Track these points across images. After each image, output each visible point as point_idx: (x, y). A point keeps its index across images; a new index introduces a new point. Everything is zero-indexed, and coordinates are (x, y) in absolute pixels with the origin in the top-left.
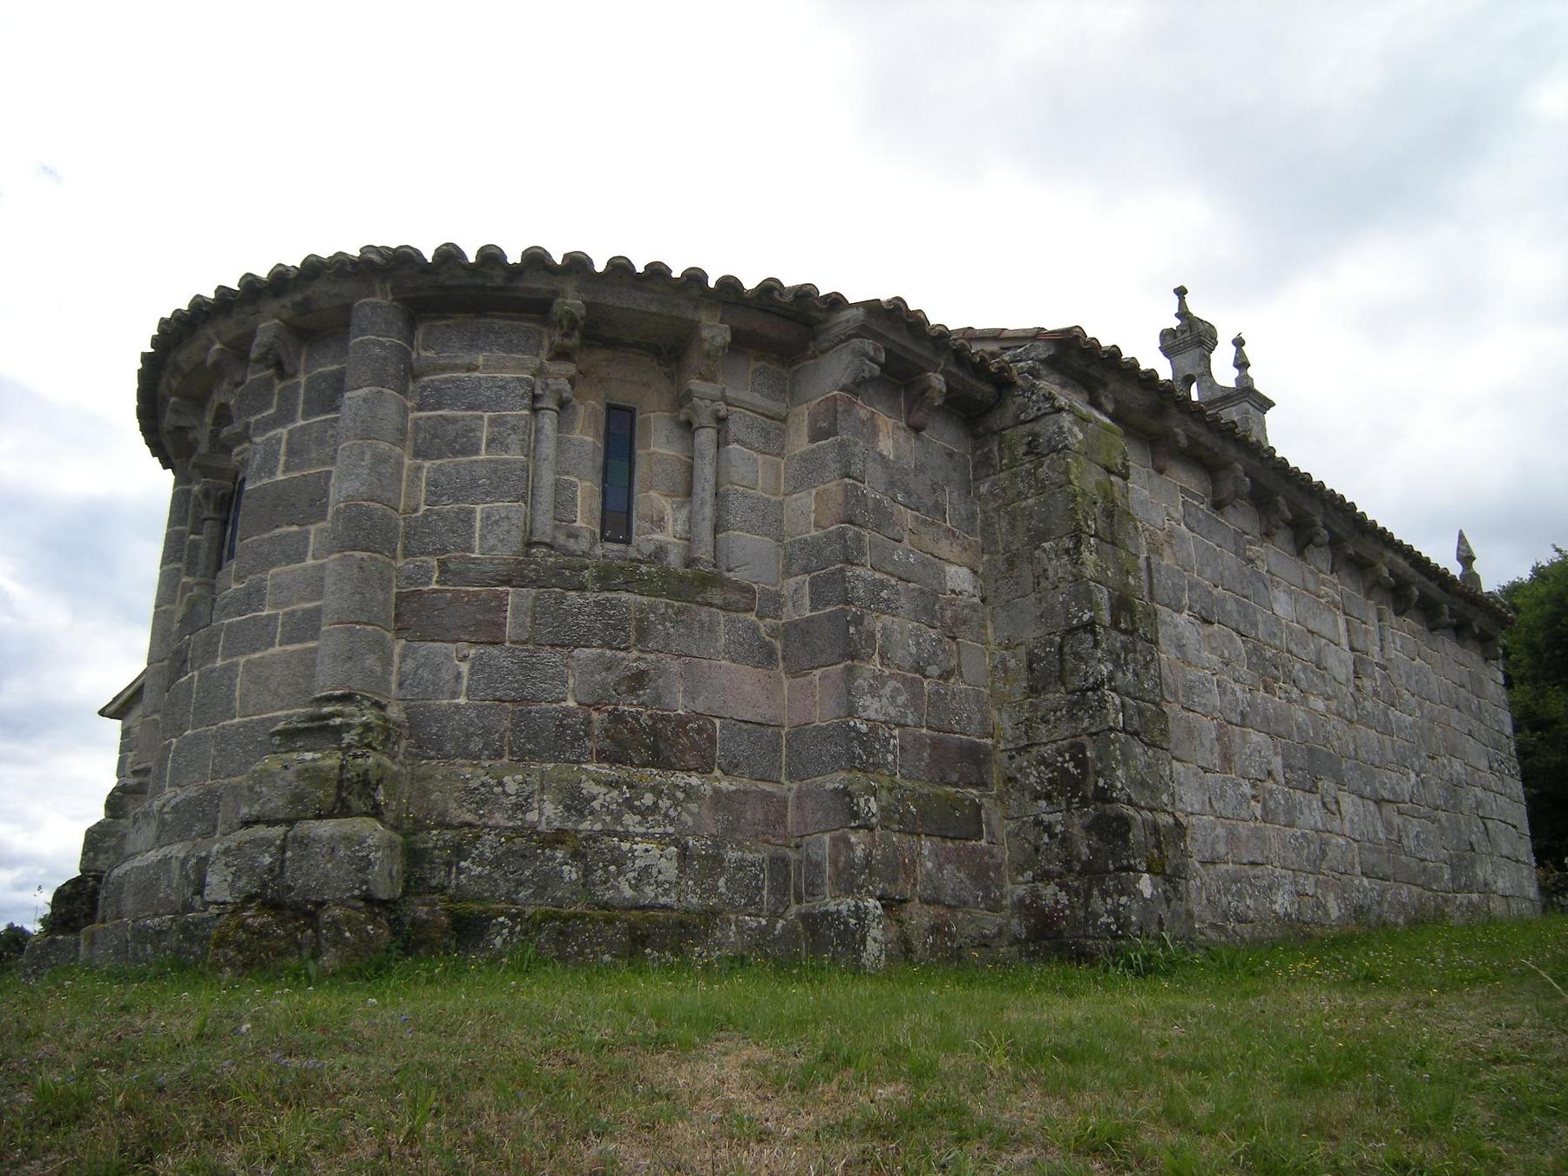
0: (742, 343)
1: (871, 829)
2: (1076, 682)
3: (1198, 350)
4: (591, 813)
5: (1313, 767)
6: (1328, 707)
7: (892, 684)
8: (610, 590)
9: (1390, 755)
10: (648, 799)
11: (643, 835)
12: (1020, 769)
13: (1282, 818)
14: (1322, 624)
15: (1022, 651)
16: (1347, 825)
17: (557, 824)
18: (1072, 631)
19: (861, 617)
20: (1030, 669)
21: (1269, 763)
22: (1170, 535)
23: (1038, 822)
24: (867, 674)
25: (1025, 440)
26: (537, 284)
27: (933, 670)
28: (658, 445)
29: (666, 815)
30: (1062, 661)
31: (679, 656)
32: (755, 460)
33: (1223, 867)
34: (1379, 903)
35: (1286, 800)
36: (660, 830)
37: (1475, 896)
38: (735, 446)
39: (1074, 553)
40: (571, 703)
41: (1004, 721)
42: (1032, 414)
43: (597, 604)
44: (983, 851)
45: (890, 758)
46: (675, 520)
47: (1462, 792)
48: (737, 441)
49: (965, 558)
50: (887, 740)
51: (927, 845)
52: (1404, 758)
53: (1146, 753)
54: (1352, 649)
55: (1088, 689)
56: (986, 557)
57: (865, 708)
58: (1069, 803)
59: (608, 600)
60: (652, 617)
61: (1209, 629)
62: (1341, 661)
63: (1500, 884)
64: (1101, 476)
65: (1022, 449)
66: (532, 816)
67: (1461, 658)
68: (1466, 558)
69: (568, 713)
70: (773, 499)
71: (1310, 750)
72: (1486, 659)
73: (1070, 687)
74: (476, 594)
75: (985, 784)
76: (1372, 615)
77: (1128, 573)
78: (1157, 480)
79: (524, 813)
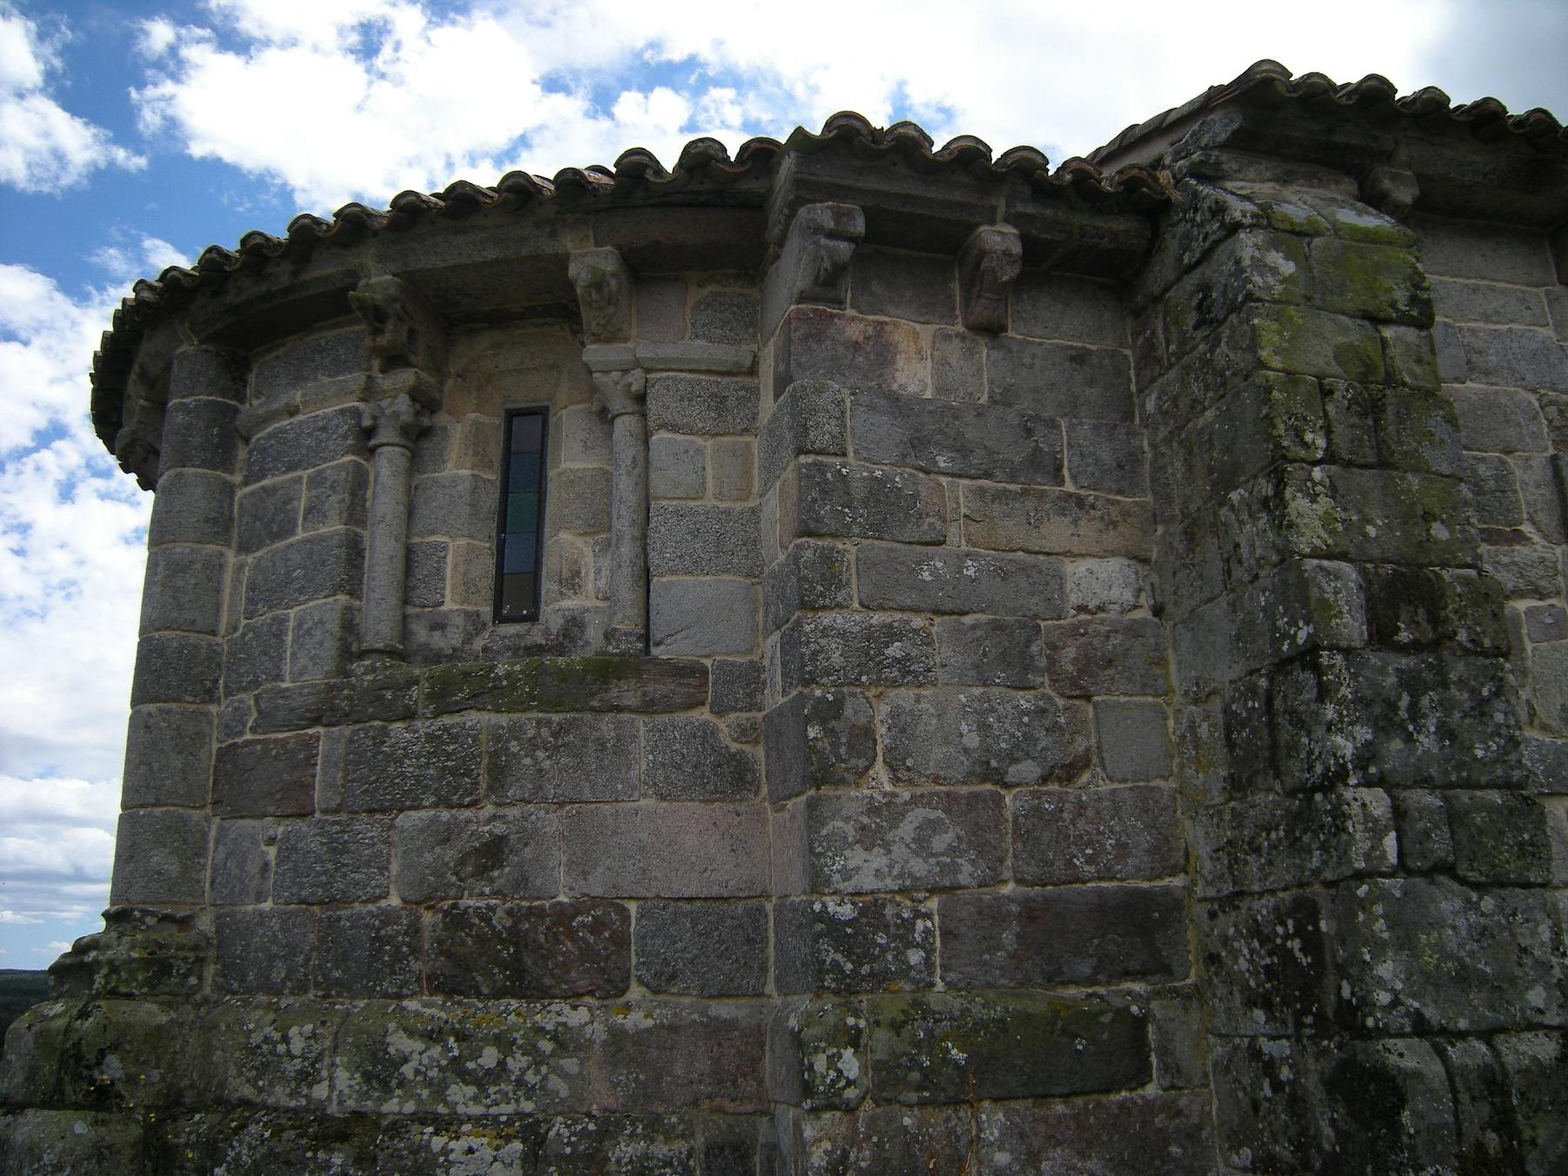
0: (647, 270)
1: (850, 1109)
2: (1295, 771)
4: (401, 1085)
7: (918, 815)
8: (451, 712)
10: (490, 1057)
11: (478, 1121)
12: (1225, 941)
15: (1216, 705)
17: (351, 1103)
18: (1283, 666)
19: (838, 705)
20: (1230, 744)
23: (1255, 1053)
24: (851, 808)
25: (1194, 302)
26: (325, 269)
27: (1027, 770)
28: (572, 457)
29: (520, 1083)
30: (1272, 727)
31: (561, 805)
32: (699, 451)
36: (509, 1109)
38: (664, 434)
39: (1274, 506)
40: (394, 901)
41: (1198, 838)
42: (1198, 247)
43: (431, 737)
44: (1149, 1107)
45: (915, 957)
46: (598, 571)
48: (663, 426)
49: (1112, 539)
50: (909, 925)
51: (993, 1120)
53: (1470, 906)
55: (1316, 788)
56: (1160, 530)
57: (847, 874)
58: (1299, 1025)
59: (446, 729)
60: (514, 746)
64: (1354, 334)
65: (1191, 319)
66: (320, 1091)
69: (388, 917)
70: (739, 506)
73: (1288, 781)
74: (285, 741)
75: (1167, 970)
77: (1428, 517)
79: (310, 1086)
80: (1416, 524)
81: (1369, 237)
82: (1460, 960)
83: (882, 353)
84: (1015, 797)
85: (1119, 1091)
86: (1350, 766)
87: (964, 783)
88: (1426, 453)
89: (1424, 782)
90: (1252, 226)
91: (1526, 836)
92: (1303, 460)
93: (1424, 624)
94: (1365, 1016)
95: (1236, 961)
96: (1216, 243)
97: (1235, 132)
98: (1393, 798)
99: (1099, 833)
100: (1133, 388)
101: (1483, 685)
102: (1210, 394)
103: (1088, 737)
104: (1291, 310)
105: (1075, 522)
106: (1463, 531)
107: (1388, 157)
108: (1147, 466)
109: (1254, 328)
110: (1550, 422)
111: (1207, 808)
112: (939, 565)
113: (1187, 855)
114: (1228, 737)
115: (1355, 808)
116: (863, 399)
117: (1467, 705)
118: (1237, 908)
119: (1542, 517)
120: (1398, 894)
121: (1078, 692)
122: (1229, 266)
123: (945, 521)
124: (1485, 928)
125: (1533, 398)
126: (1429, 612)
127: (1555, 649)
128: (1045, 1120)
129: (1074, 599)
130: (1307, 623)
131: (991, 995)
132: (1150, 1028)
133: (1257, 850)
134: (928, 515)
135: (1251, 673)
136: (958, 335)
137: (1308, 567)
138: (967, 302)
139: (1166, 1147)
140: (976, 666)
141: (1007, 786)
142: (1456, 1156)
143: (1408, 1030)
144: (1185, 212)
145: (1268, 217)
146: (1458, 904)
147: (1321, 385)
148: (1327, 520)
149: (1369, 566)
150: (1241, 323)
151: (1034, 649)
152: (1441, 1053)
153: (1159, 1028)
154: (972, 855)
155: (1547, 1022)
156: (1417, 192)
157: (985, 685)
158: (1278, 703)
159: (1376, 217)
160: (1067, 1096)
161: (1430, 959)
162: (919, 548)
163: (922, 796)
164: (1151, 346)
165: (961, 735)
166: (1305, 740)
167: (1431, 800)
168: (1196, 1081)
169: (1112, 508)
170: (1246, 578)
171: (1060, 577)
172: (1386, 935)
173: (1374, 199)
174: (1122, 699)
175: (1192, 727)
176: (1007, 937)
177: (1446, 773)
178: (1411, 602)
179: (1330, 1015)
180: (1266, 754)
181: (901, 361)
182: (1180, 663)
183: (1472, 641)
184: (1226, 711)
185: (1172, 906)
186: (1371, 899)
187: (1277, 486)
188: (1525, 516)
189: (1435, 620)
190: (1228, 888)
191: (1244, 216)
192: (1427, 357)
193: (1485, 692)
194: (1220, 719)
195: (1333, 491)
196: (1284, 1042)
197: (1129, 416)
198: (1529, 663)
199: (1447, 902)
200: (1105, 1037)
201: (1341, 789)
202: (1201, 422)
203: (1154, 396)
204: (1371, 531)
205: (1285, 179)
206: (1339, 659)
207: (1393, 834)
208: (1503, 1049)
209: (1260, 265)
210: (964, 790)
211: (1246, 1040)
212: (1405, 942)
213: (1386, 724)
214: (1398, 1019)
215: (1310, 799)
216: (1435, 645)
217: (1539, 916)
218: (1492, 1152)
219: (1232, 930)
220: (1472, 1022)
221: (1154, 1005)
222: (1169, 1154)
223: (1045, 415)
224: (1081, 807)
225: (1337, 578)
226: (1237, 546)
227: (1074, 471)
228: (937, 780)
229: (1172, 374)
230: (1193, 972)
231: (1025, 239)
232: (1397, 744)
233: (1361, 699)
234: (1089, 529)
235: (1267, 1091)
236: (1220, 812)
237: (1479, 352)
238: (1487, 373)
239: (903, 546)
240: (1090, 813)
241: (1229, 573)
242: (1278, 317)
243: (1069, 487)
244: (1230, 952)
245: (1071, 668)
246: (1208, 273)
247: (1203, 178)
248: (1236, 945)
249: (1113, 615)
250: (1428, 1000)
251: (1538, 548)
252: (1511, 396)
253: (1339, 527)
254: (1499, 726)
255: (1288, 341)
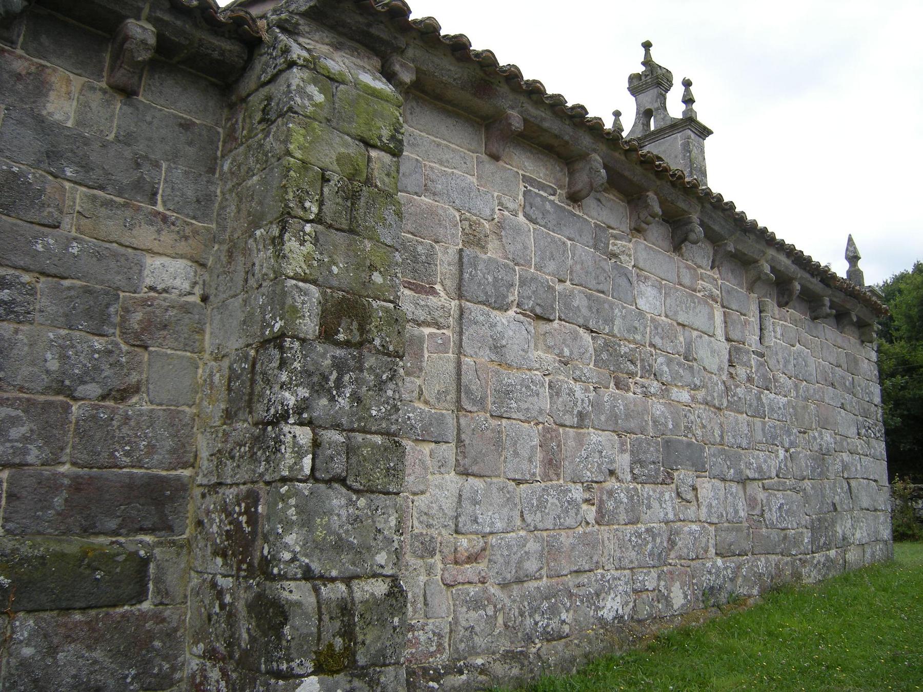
2: (260, 412)
3: (656, 90)
5: (668, 458)
6: (693, 398)
9: (759, 436)
12: (208, 512)
13: (623, 517)
14: (699, 319)
15: (226, 363)
16: (704, 510)
20: (229, 389)
21: (612, 462)
22: (501, 226)
23: (214, 585)
27: (92, 390)
30: (253, 382)
33: (532, 585)
34: (732, 580)
35: (631, 498)
37: (832, 553)
39: (277, 242)
42: (271, 71)
44: (143, 616)
47: (829, 460)
52: (774, 437)
53: (351, 503)
54: (728, 340)
55: (270, 423)
61: (544, 327)
62: (713, 351)
63: (858, 535)
64: (353, 149)
65: (258, 116)
67: (839, 341)
68: (853, 258)
71: (667, 443)
72: (863, 342)
75: (170, 529)
76: (754, 308)
77: (372, 268)
78: (490, 166)
80: (364, 271)
81: (375, 94)
82: (339, 535)
83: (40, 87)
84: (79, 407)
85: (123, 605)
86: (291, 412)
87: (42, 394)
88: (380, 230)
89: (337, 426)
90: (302, 66)
91: (392, 465)
92: (301, 218)
93: (355, 331)
94: (273, 567)
95: (211, 527)
96: (281, 72)
97: (311, 7)
98: (315, 434)
99: (136, 436)
100: (219, 154)
101: (384, 372)
102: (258, 166)
103: (141, 373)
104: (316, 124)
105: (159, 232)
106: (391, 280)
107: (402, 52)
108: (217, 205)
109: (289, 129)
110: (464, 230)
111: (211, 427)
112: (51, 241)
113: (196, 456)
114: (229, 385)
115: (289, 437)
116: (14, 114)
117: (372, 384)
118: (217, 493)
119: (448, 283)
120: (306, 493)
121: (138, 343)
122: (284, 88)
123: (61, 212)
124: (358, 516)
125: (457, 214)
126: (359, 324)
127: (440, 358)
128: (65, 625)
129: (148, 281)
130: (281, 319)
131: (39, 539)
132: (152, 565)
133: (233, 458)
134: (49, 206)
135: (248, 346)
136: (101, 89)
137: (289, 285)
138: (112, 69)
139: (151, 642)
140: (66, 315)
141: (75, 399)
142: (315, 653)
143: (299, 576)
144: (269, 48)
145: (315, 64)
146: (343, 501)
147: (323, 175)
148: (308, 258)
149: (329, 291)
150: (283, 125)
151: (112, 310)
152: (316, 590)
153: (158, 566)
154: (40, 443)
155: (385, 573)
156: (414, 78)
157: (70, 329)
158: (258, 366)
159: (384, 83)
160: (84, 609)
161: (320, 534)
162: (37, 227)
163: (8, 399)
164: (233, 129)
165: (46, 361)
166: (268, 392)
167: (337, 437)
168: (178, 600)
169: (186, 228)
170: (255, 286)
171: (141, 266)
172: (294, 518)
173: (389, 75)
174: (169, 352)
175: (211, 375)
176: (58, 501)
177: (352, 422)
178: (350, 317)
179: (256, 565)
180: (247, 398)
181: (52, 95)
182: (211, 333)
183: (383, 346)
184: (230, 368)
185: (180, 488)
186: (288, 495)
187: (281, 231)
188: (439, 280)
189: (362, 329)
190: (214, 480)
191: (299, 59)
192: (394, 174)
193: (384, 377)
194: (226, 372)
195: (316, 241)
196: (230, 579)
197: (212, 171)
198: (424, 364)
199: (337, 499)
200: (118, 570)
201: (282, 424)
202: (250, 183)
203: (229, 161)
204: (335, 269)
205: (337, 47)
206: (297, 344)
207: (310, 456)
208: (355, 588)
209: (301, 91)
210: (42, 398)
211: (211, 576)
212: (307, 522)
213: (320, 387)
214: (294, 569)
215: (265, 430)
216: (360, 345)
217: (391, 511)
218: (337, 649)
219: (212, 506)
220: (340, 572)
221: (157, 551)
222: (153, 646)
223: (152, 157)
224: (127, 419)
225: (306, 294)
226: (254, 264)
227: (165, 199)
228: (21, 389)
229: (241, 149)
230: (187, 531)
231: (160, 37)
232: (324, 401)
233: (306, 371)
234: (167, 237)
235: (217, 609)
236: (217, 431)
237: (433, 181)
238: (434, 194)
239: (25, 224)
240: (132, 423)
241: (246, 281)
242: (306, 127)
243: (160, 208)
244: (209, 520)
245: (136, 326)
246: (273, 90)
247: (284, 30)
248: (213, 516)
249: (173, 296)
250: (315, 559)
251: (442, 299)
252: (445, 210)
253: (315, 263)
254: (389, 398)
255: (310, 143)
